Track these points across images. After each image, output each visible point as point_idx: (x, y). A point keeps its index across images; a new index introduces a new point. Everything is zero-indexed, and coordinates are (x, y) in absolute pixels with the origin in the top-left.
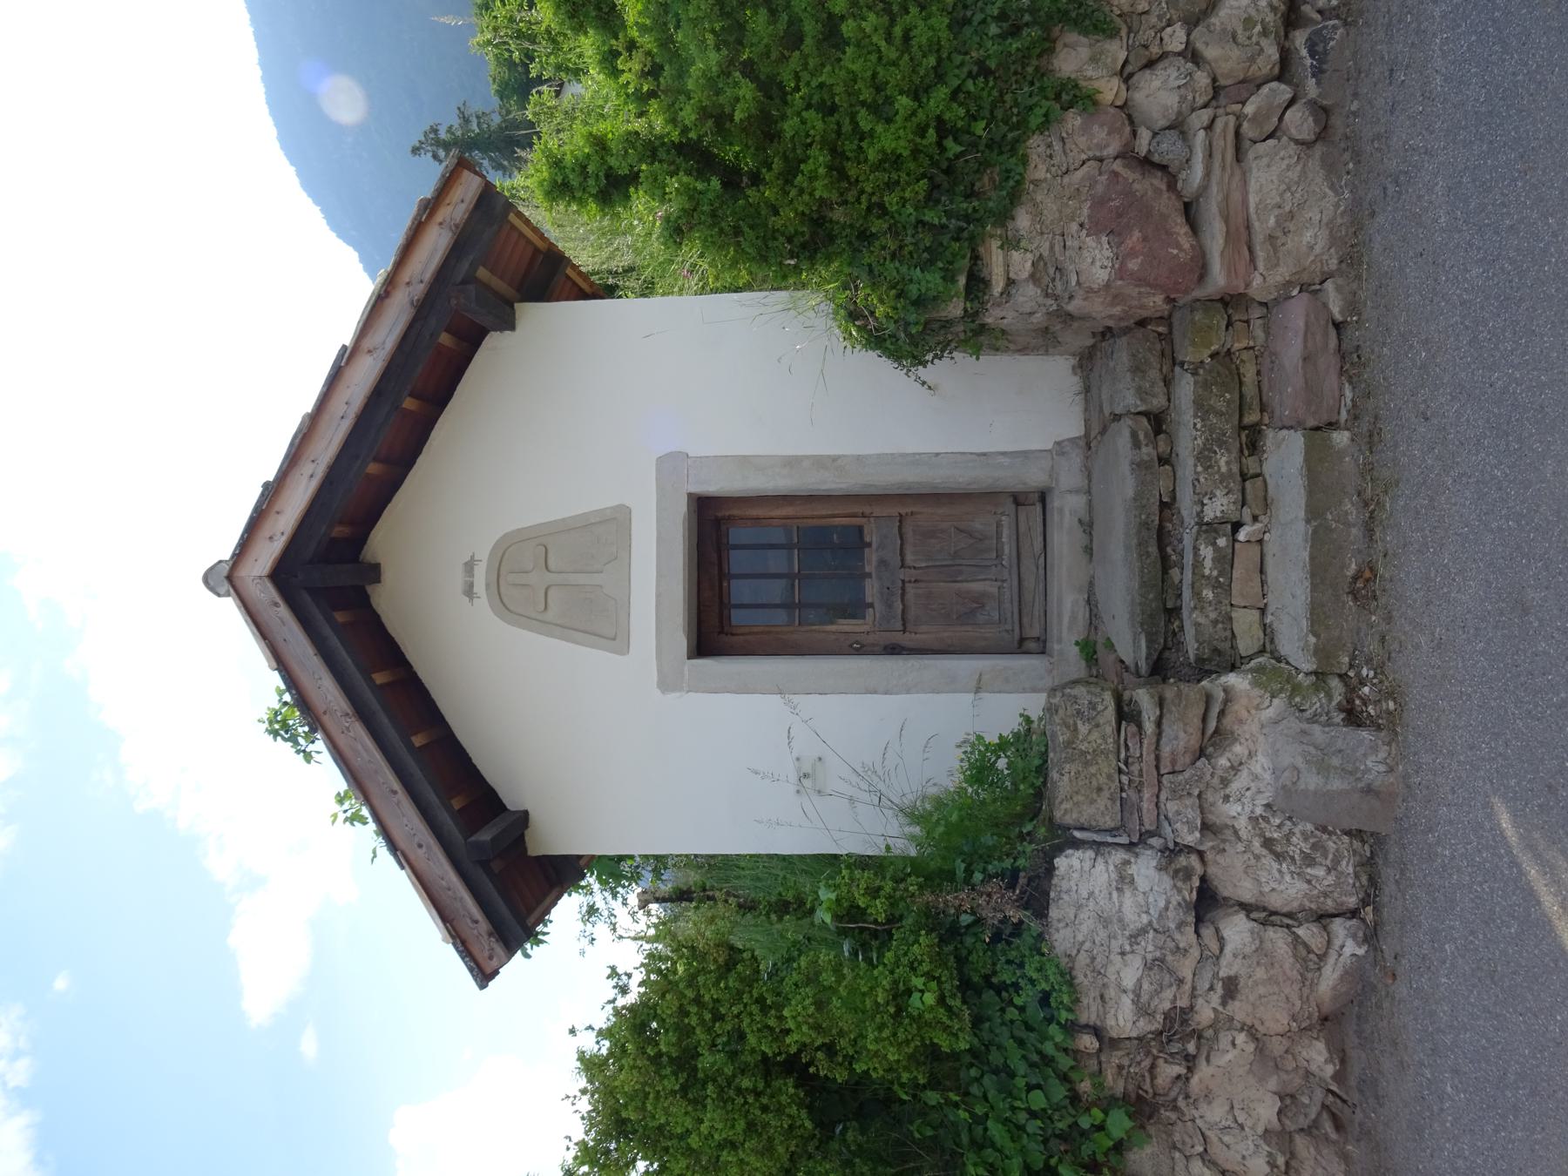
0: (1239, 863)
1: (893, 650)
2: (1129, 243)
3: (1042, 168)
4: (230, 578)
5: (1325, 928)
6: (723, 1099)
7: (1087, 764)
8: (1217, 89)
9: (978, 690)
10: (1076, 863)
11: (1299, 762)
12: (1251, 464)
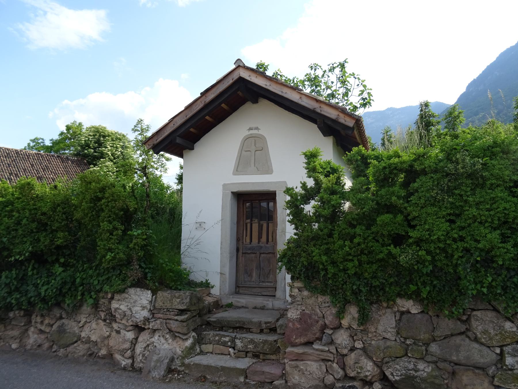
0: (145, 338)
1: (238, 250)
2: (296, 324)
3: (321, 300)
4: (239, 66)
5: (129, 358)
6: (90, 208)
7: (170, 300)
8: (344, 356)
9: (221, 273)
10: (149, 296)
11: (160, 355)
12: (250, 355)
